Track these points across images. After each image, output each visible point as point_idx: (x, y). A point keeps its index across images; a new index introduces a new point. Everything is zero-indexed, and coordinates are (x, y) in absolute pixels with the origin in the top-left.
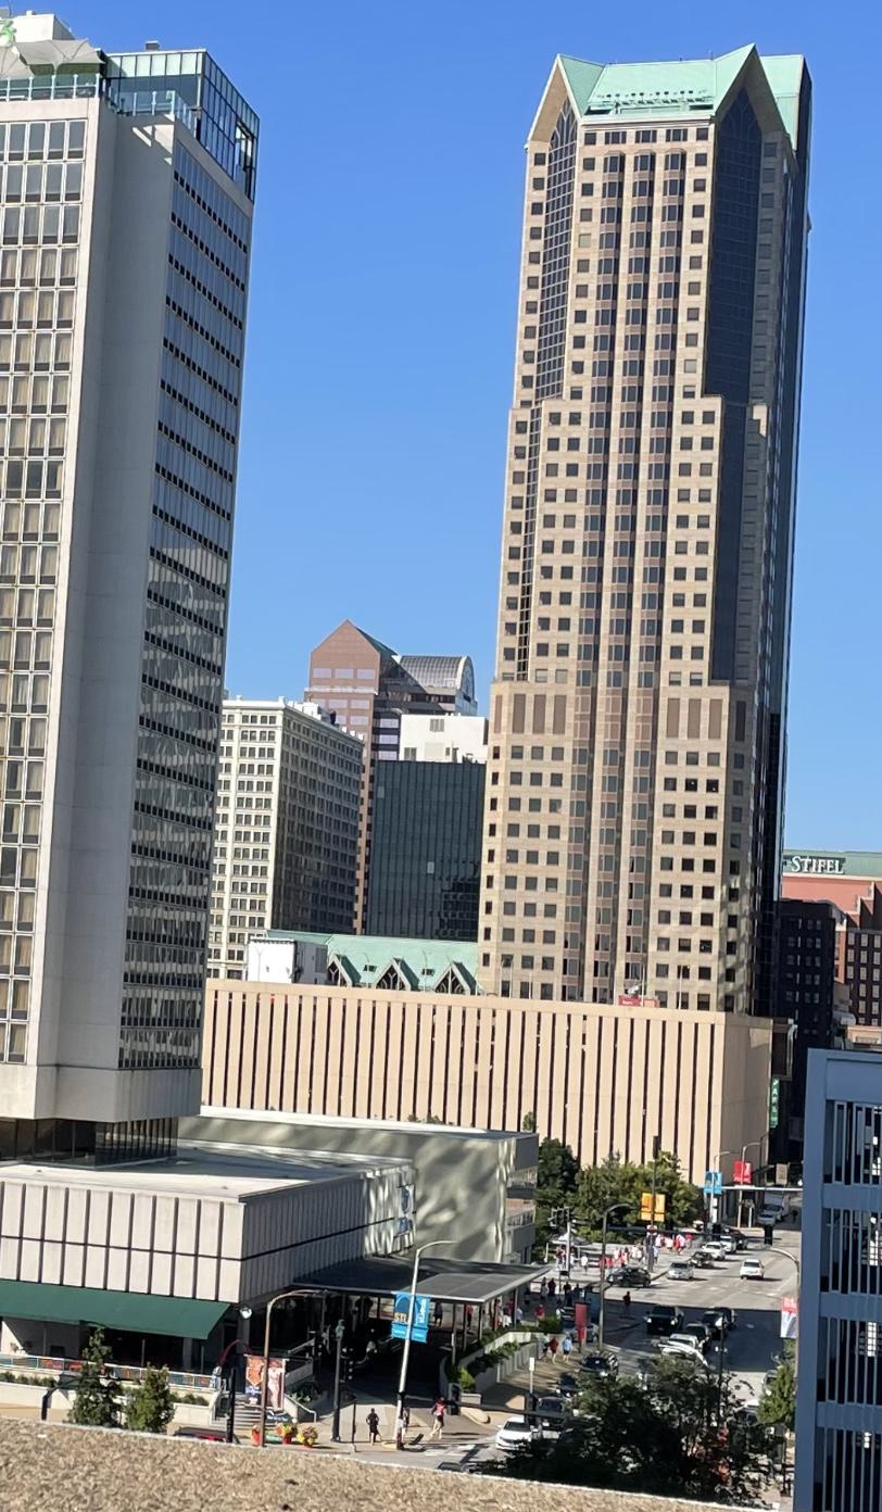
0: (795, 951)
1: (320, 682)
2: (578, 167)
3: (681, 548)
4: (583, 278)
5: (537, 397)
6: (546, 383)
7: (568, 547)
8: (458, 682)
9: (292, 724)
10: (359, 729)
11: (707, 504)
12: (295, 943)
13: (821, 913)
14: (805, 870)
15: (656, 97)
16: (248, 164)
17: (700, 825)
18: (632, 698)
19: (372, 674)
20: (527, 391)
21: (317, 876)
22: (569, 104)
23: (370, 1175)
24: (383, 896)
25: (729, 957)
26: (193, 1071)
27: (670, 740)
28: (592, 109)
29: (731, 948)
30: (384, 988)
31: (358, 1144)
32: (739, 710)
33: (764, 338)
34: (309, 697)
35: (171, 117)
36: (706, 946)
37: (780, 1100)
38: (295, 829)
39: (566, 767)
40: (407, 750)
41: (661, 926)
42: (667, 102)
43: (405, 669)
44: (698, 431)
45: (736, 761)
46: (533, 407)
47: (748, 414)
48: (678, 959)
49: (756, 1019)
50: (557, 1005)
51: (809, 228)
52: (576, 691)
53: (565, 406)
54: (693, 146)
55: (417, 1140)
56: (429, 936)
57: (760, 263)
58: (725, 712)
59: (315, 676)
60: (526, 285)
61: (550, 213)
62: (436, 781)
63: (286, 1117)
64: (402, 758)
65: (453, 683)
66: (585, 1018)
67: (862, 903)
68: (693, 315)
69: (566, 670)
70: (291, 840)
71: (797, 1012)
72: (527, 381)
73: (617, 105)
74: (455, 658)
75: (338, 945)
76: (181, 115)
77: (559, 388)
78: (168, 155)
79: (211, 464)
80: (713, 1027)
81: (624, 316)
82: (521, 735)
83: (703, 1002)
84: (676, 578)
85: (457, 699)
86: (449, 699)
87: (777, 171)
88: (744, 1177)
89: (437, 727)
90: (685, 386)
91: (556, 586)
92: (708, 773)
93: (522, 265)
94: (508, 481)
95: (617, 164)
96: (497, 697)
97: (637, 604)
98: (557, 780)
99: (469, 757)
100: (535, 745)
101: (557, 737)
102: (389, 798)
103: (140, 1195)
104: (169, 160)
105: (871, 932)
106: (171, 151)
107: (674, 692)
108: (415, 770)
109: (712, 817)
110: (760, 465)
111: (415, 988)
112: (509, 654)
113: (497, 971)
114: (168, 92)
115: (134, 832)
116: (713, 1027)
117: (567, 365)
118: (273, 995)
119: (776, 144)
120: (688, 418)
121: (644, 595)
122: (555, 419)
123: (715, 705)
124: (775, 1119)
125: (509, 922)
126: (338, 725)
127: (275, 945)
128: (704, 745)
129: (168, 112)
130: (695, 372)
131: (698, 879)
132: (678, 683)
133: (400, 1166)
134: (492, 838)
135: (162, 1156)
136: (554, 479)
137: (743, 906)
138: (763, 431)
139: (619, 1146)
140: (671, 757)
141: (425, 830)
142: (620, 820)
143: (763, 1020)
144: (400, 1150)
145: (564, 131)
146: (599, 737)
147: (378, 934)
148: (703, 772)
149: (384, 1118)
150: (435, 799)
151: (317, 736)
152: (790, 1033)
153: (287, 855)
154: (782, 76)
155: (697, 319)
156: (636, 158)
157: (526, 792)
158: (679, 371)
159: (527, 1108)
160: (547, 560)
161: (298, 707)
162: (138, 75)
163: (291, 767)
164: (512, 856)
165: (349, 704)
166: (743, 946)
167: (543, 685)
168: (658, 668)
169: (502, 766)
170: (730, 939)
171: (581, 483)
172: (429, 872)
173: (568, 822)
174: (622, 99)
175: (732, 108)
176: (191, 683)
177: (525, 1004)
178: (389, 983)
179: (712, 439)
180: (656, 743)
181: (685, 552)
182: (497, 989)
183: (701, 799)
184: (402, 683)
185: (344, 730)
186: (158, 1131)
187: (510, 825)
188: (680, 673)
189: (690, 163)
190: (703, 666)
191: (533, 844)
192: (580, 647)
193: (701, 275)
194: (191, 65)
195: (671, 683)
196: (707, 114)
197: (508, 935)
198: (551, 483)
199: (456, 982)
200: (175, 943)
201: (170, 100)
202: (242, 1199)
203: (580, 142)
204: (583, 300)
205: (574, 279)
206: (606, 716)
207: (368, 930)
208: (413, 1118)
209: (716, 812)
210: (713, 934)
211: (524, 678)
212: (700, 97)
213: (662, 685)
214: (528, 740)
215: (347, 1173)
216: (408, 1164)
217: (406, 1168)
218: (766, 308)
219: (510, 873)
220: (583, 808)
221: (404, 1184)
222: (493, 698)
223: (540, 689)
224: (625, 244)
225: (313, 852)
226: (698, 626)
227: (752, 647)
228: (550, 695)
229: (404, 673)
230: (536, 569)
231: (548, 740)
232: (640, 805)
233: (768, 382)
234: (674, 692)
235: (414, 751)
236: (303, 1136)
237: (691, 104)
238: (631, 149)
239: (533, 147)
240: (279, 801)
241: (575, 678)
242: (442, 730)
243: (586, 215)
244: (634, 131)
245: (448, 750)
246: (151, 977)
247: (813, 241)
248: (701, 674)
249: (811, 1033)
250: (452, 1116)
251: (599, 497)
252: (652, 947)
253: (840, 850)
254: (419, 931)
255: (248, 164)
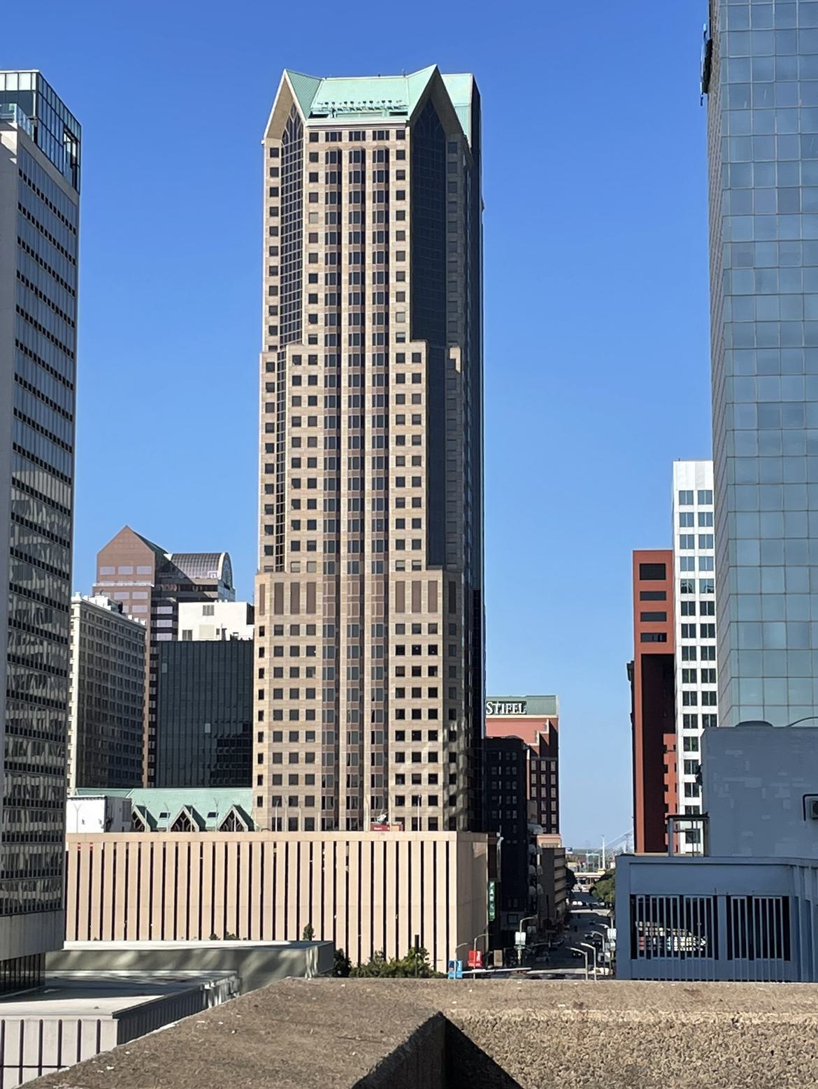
0: (497, 778)
1: (105, 578)
2: (306, 159)
3: (400, 461)
4: (314, 248)
5: (281, 342)
6: (289, 330)
7: (312, 463)
8: (219, 573)
9: (88, 615)
10: (141, 616)
11: (419, 426)
12: (106, 798)
13: (515, 744)
14: (496, 712)
15: (363, 105)
16: (74, 162)
17: (425, 682)
18: (368, 583)
19: (150, 570)
20: (273, 338)
21: (112, 741)
22: (295, 109)
23: (207, 987)
24: (169, 754)
25: (451, 786)
26: (57, 912)
27: (399, 615)
28: (314, 113)
29: (452, 779)
30: (177, 831)
31: (192, 963)
32: (450, 588)
33: (456, 296)
34: (97, 591)
35: (14, 125)
36: (433, 779)
37: (495, 899)
38: (93, 703)
39: (318, 641)
40: (184, 632)
41: (399, 764)
42: (372, 109)
43: (176, 564)
44: (409, 368)
45: (450, 629)
46: (279, 351)
47: (446, 355)
48: (413, 791)
49: (477, 834)
50: (318, 835)
51: (483, 208)
52: (324, 578)
53: (305, 350)
54: (394, 144)
55: (241, 954)
56: (183, 785)
57: (450, 237)
58: (440, 590)
59: (101, 574)
60: (268, 253)
61: (285, 195)
62: (209, 657)
63: (132, 944)
64: (180, 638)
65: (216, 575)
66: (348, 843)
67: (540, 735)
68: (400, 277)
69: (315, 562)
70: (89, 712)
71: (500, 827)
72: (273, 330)
73: (334, 110)
74: (216, 554)
75: (141, 797)
76: (22, 123)
77: (299, 335)
78: (14, 156)
79: (56, 407)
80: (447, 843)
81: (347, 278)
82: (281, 616)
83: (433, 824)
84: (397, 486)
85: (219, 587)
86: (213, 588)
87: (459, 165)
88: (476, 962)
89: (208, 612)
90: (397, 333)
91: (304, 494)
92: (429, 640)
93: (264, 237)
94: (262, 411)
95: (335, 157)
96: (261, 586)
97: (368, 507)
98: (311, 651)
99: (236, 635)
100: (293, 623)
101: (310, 616)
102: (171, 673)
103: (28, 1021)
104: (14, 160)
105: (548, 759)
106: (15, 153)
107: (400, 576)
108: (191, 647)
109: (311, 676)
110: (456, 394)
111: (154, 829)
112: (268, 550)
113: (269, 811)
114: (11, 105)
115: (7, 712)
116: (447, 843)
117: (305, 317)
118: (91, 843)
119: (456, 143)
120: (400, 358)
121: (373, 500)
122: (297, 360)
123: (432, 585)
124: (493, 914)
125: (278, 768)
126: (124, 614)
127: (89, 801)
128: (425, 618)
129: (12, 120)
130: (404, 322)
131: (425, 725)
132: (403, 569)
133: (228, 976)
134: (261, 701)
135: (34, 987)
136: (298, 408)
137: (460, 745)
138: (458, 368)
139: (378, 947)
140: (400, 629)
141: (203, 698)
142: (362, 681)
143: (482, 835)
144: (228, 964)
145: (294, 129)
146: (343, 615)
147: (166, 786)
148: (425, 640)
149: (188, 939)
150: (209, 671)
151: (108, 623)
152: (499, 844)
153: (87, 724)
154: (459, 89)
155: (404, 280)
156: (350, 153)
157: (287, 662)
158: (392, 321)
159: (304, 923)
160: (297, 473)
161: (92, 601)
162: (21, 89)
163: (87, 651)
164: (278, 715)
165: (131, 595)
166: (461, 777)
167: (298, 574)
168: (387, 558)
169: (266, 642)
170: (452, 772)
171: (320, 411)
172: (206, 732)
173: (321, 685)
174: (337, 106)
175: (421, 116)
176: (47, 584)
177: (434, 835)
178: (181, 826)
179: (420, 374)
180: (339, 619)
181: (404, 465)
182: (268, 825)
183: (425, 661)
184: (173, 577)
185: (130, 617)
186: (25, 965)
187: (275, 690)
188: (404, 561)
189: (392, 158)
190: (421, 555)
191: (294, 704)
192: (325, 542)
193: (405, 246)
194: (26, 82)
195: (398, 569)
196: (403, 119)
197: (277, 780)
198: (296, 412)
199: (188, 822)
200: (37, 806)
201: (13, 111)
202: (115, 1015)
203: (306, 139)
204: (315, 265)
205: (307, 248)
206: (348, 598)
207: (154, 782)
208: (213, 937)
209: (437, 670)
210: (438, 768)
211: (281, 569)
212: (397, 105)
213: (390, 571)
214: (287, 619)
215: (191, 987)
216: (234, 975)
217: (233, 978)
218: (456, 272)
219: (277, 729)
220: (332, 673)
221: (232, 992)
222: (257, 586)
223: (295, 578)
224: (345, 221)
225: (108, 721)
226: (416, 523)
227: (459, 538)
228: (303, 583)
229: (175, 568)
230: (288, 481)
231: (303, 619)
232: (377, 668)
233: (460, 330)
234: (400, 576)
235: (190, 632)
236: (147, 959)
237: (391, 111)
238: (346, 146)
239: (268, 143)
240: (79, 680)
241: (322, 568)
242: (213, 614)
243: (314, 197)
244: (348, 132)
245: (218, 630)
246: (23, 836)
247: (487, 219)
248: (420, 561)
249: (512, 841)
250: (244, 932)
251: (334, 422)
252: (392, 782)
253: (522, 695)
254: (188, 782)
255: (74, 162)
